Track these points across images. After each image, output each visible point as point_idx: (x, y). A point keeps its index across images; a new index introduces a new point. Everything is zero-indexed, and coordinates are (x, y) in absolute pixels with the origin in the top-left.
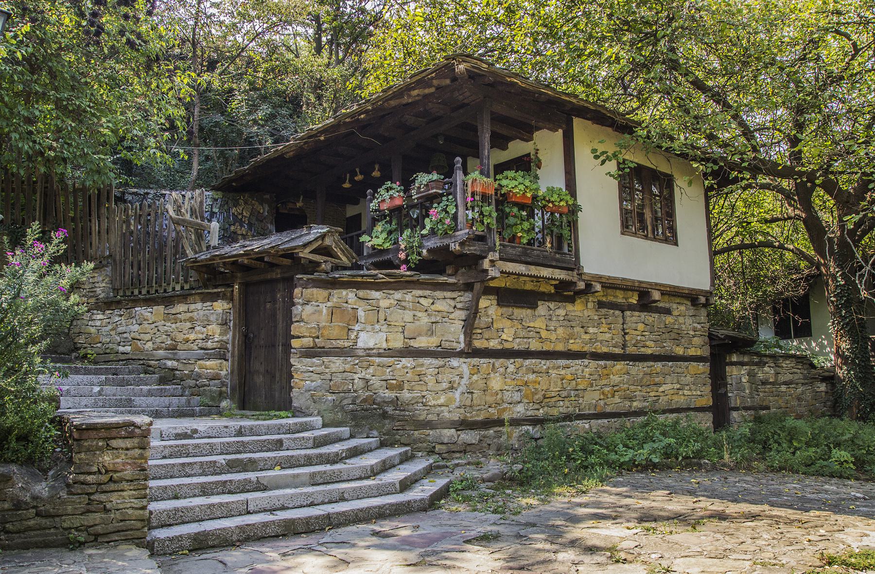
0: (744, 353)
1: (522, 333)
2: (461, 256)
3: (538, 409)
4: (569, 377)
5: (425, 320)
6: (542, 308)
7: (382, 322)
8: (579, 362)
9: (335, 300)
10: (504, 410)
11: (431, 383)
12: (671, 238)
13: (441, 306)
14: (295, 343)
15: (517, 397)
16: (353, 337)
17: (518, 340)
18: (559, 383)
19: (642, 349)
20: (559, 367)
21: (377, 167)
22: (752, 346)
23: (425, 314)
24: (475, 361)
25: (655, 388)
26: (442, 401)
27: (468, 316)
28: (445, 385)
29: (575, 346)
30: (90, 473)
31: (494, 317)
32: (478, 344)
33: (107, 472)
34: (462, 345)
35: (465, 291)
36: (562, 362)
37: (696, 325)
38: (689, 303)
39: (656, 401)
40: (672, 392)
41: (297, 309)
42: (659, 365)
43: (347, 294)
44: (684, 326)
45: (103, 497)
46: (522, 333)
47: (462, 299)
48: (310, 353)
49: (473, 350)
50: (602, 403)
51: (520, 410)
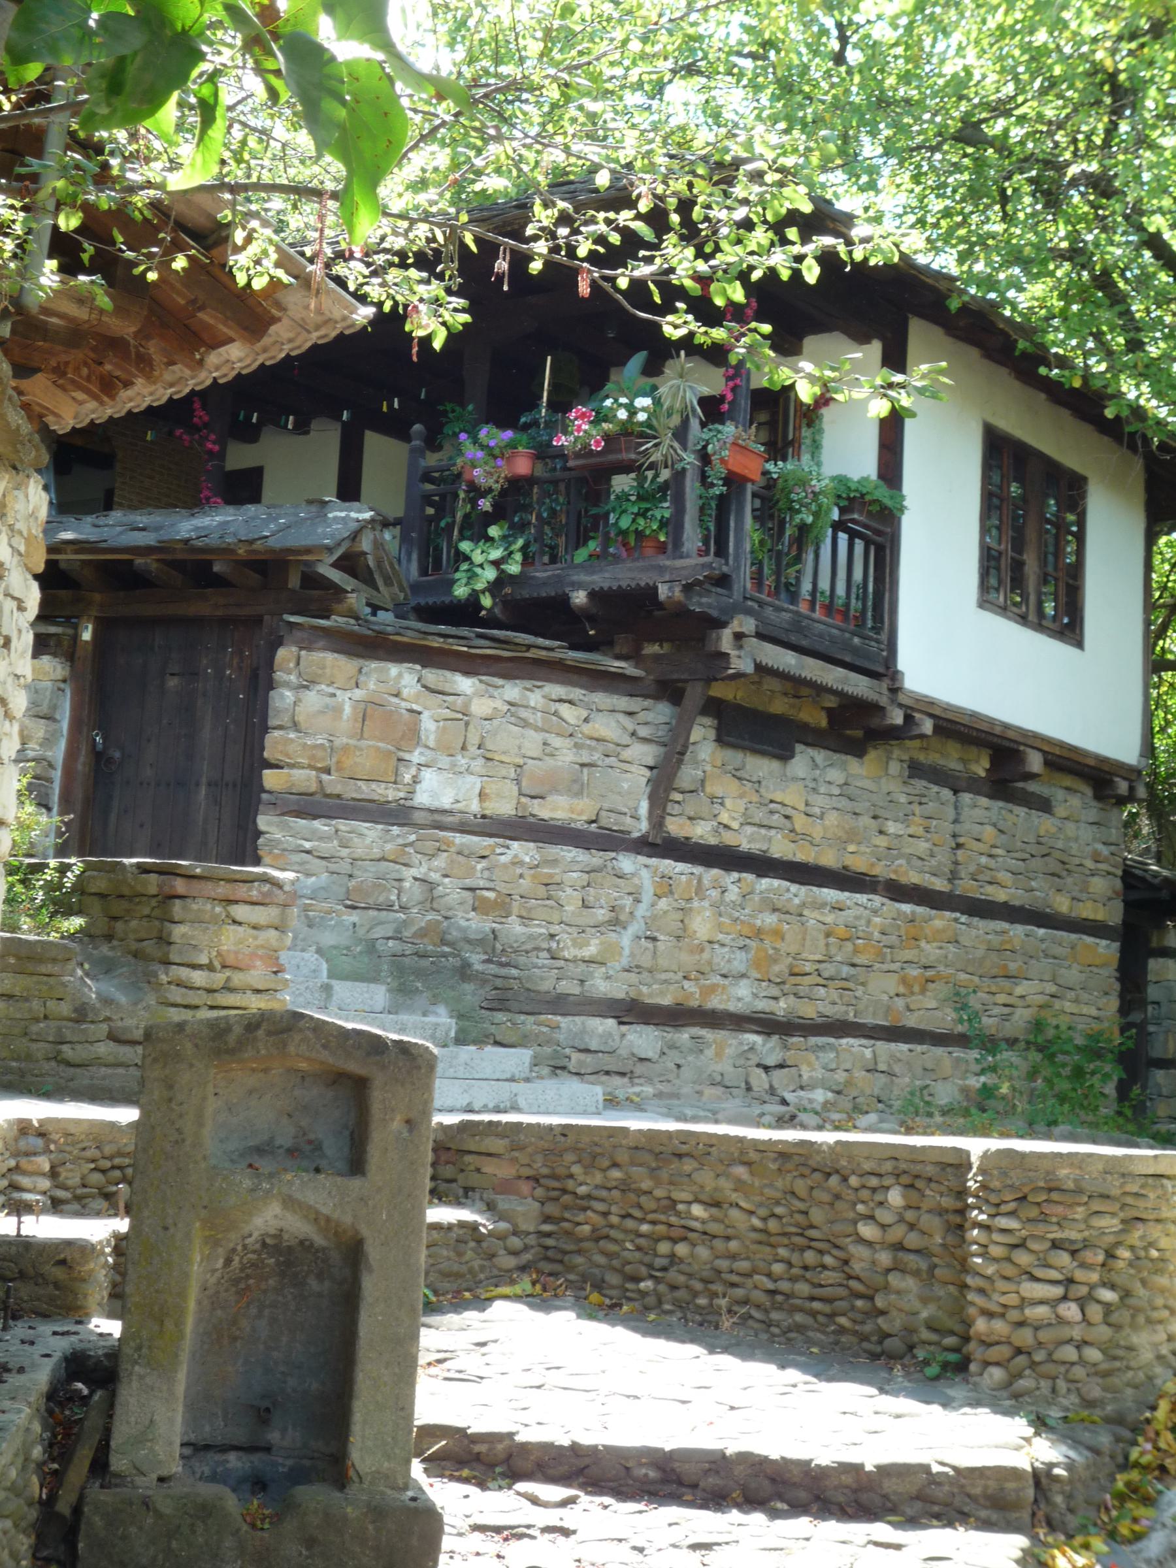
1: (759, 815)
2: (681, 613)
3: (776, 998)
4: (841, 931)
5: (567, 756)
6: (804, 760)
8: (862, 898)
9: (372, 686)
10: (713, 989)
12: (1068, 626)
14: (270, 778)
15: (740, 961)
16: (407, 778)
17: (749, 830)
18: (822, 942)
19: (990, 889)
20: (823, 905)
23: (568, 742)
24: (667, 865)
28: (602, 914)
29: (859, 863)
30: (195, 967)
31: (708, 768)
32: (675, 827)
34: (644, 826)
35: (657, 697)
36: (830, 894)
37: (1100, 847)
38: (1089, 792)
39: (1006, 1018)
40: (1040, 999)
41: (282, 696)
42: (1018, 931)
43: (400, 675)
44: (1074, 846)
46: (759, 815)
47: (649, 716)
48: (310, 806)
49: (664, 839)
50: (900, 1003)
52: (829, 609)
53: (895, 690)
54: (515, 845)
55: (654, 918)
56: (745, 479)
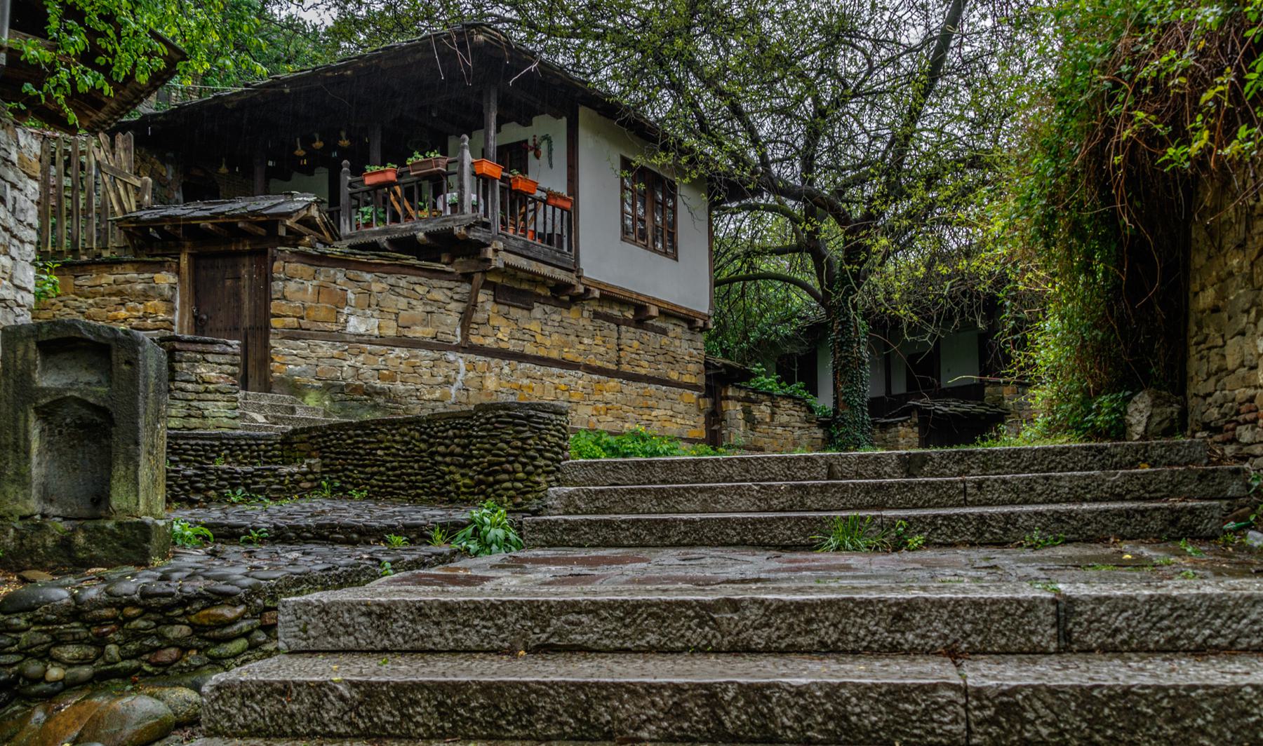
0: (740, 388)
1: (518, 335)
2: (467, 242)
8: (573, 372)
12: (671, 250)
13: (437, 295)
14: (275, 322)
21: (343, 134)
22: (748, 381)
23: (421, 302)
24: (471, 357)
25: (648, 411)
26: (437, 395)
28: (440, 379)
30: (188, 382)
32: (475, 340)
33: (204, 382)
34: (459, 339)
36: (556, 370)
38: (686, 326)
40: (664, 418)
45: (201, 405)
46: (518, 335)
47: (459, 290)
48: (294, 334)
50: (594, 419)
54: (397, 349)
55: (467, 380)
56: (494, 179)
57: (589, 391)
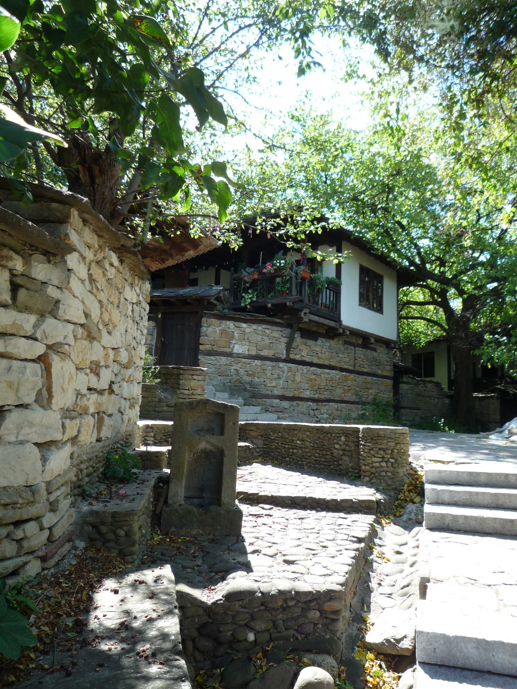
1: (311, 353)
2: (292, 309)
5: (267, 341)
6: (320, 341)
7: (246, 340)
11: (269, 373)
12: (379, 309)
14: (201, 347)
15: (307, 386)
24: (290, 365)
26: (273, 384)
27: (290, 341)
28: (276, 376)
32: (292, 356)
34: (285, 356)
36: (327, 371)
42: (369, 378)
47: (285, 332)
50: (343, 395)
51: (307, 394)
52: (325, 307)
53: (341, 324)
57: (341, 380)
